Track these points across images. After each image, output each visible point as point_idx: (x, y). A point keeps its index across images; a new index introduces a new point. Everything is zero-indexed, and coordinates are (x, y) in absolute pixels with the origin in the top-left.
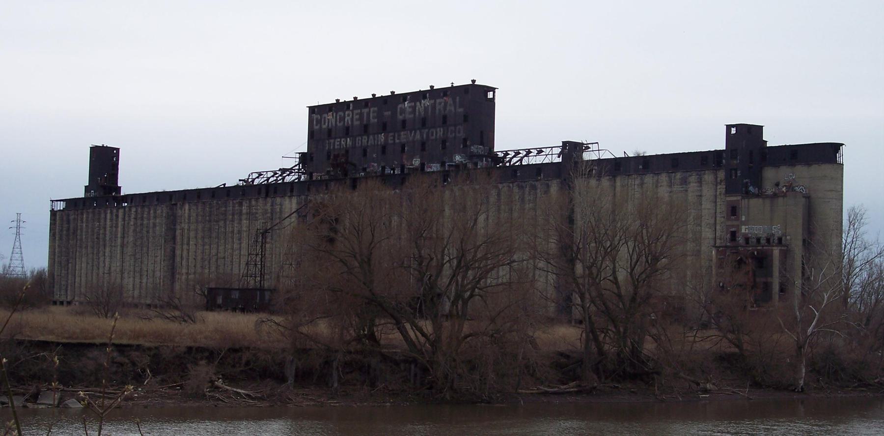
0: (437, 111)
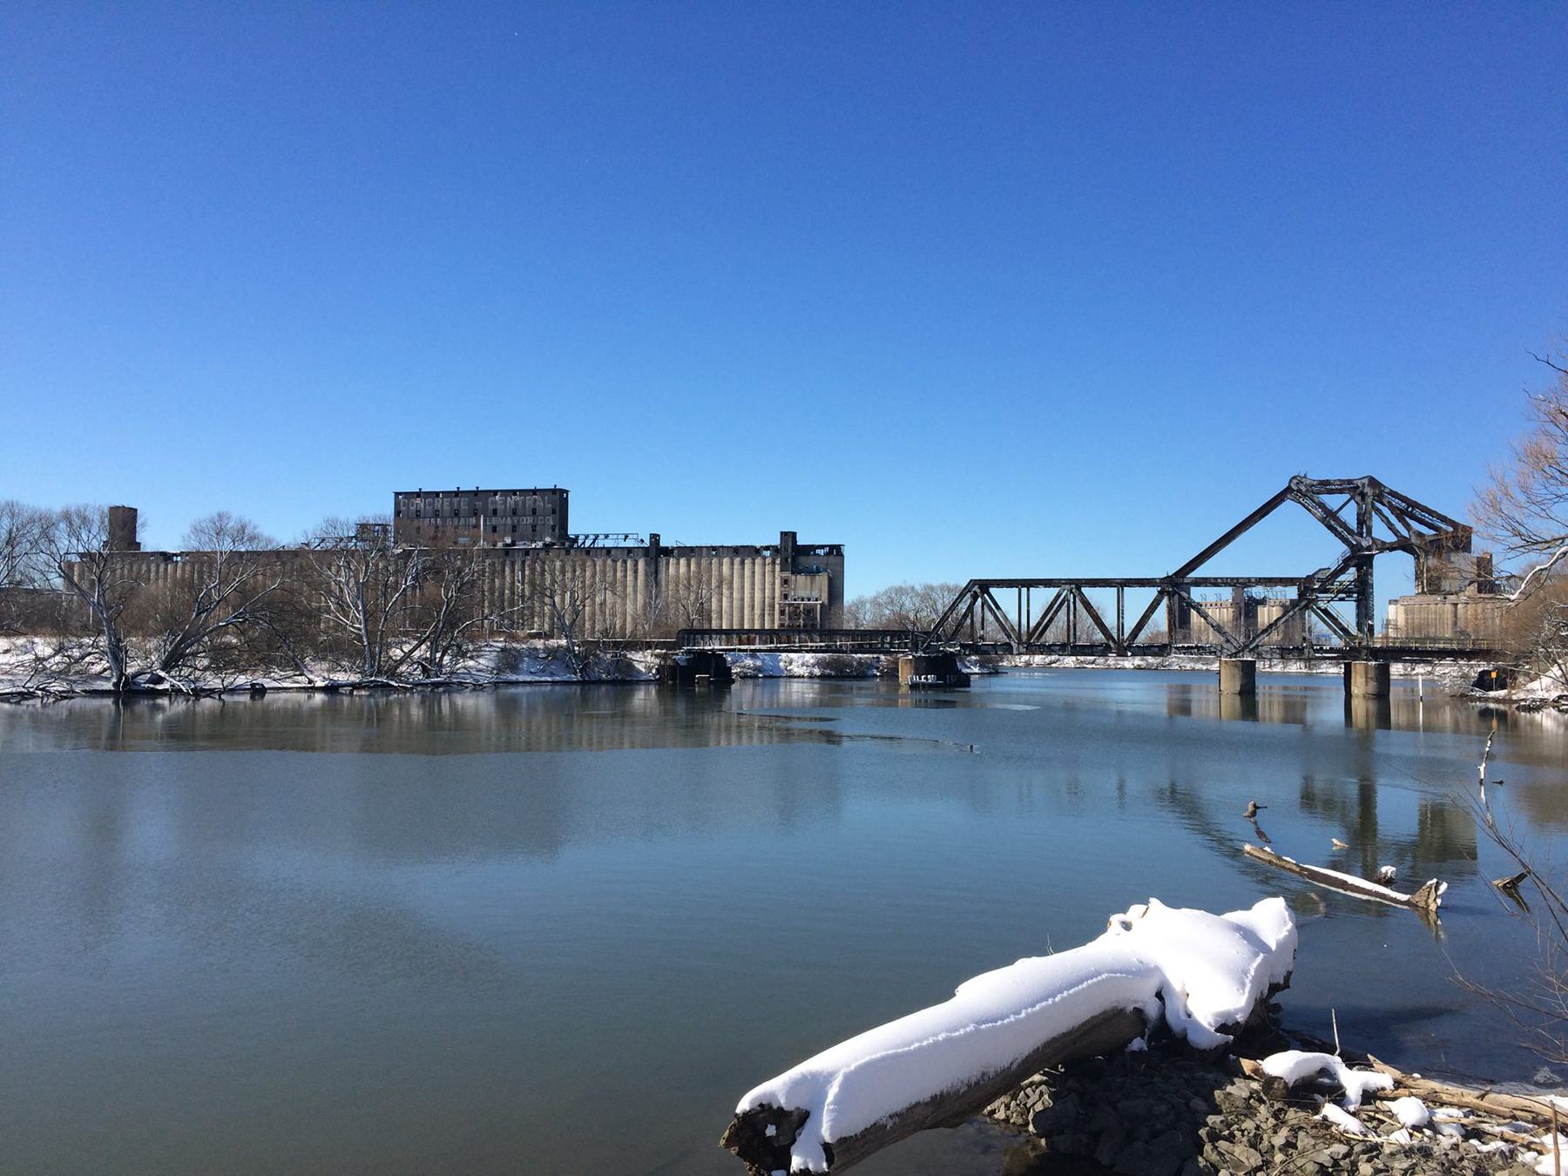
0: (527, 505)
